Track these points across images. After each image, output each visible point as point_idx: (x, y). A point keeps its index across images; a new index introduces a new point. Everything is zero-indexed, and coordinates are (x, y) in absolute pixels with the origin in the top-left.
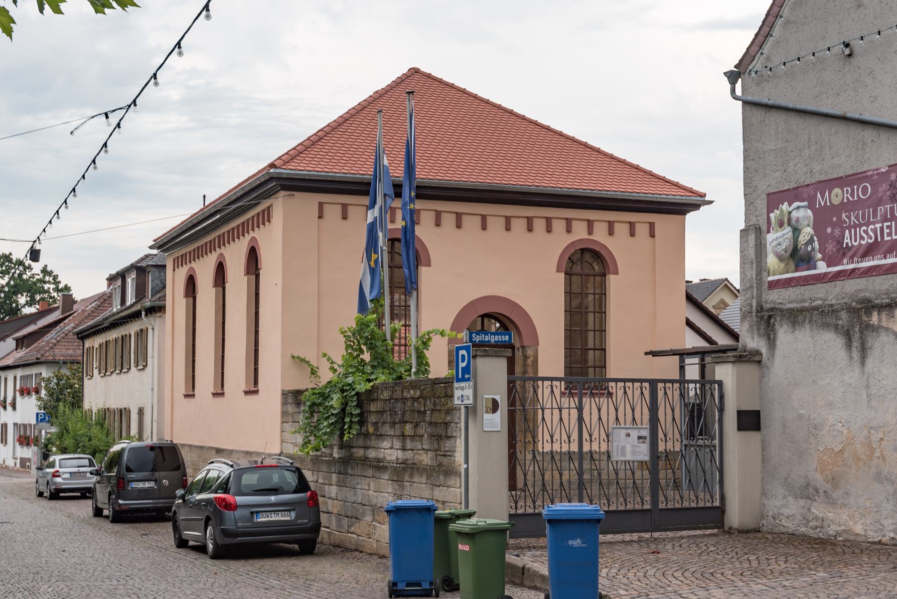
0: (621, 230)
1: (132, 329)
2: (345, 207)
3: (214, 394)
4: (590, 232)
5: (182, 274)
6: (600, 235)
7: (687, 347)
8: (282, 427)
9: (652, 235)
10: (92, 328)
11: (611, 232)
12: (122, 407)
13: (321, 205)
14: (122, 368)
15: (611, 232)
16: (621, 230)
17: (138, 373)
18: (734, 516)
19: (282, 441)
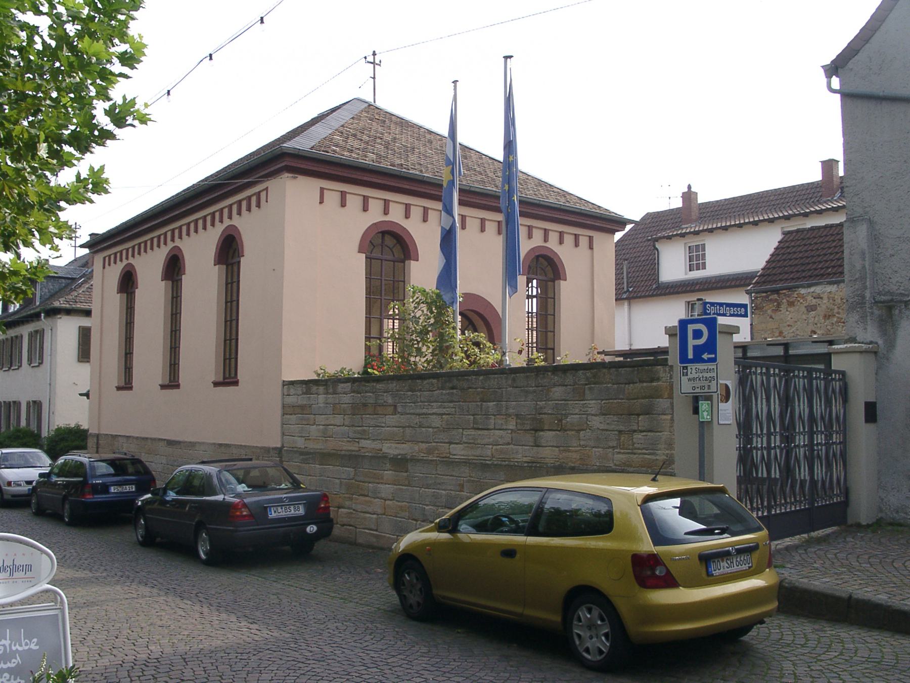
0: (569, 240)
1: (25, 331)
2: (343, 194)
3: (163, 387)
4: (546, 240)
5: (115, 272)
6: (553, 244)
7: (617, 349)
8: (282, 419)
9: (591, 247)
10: (740, 226)
11: (561, 242)
12: (11, 400)
13: (322, 189)
14: (11, 366)
15: (561, 242)
16: (569, 240)
17: (30, 370)
18: (863, 508)
19: (283, 434)
